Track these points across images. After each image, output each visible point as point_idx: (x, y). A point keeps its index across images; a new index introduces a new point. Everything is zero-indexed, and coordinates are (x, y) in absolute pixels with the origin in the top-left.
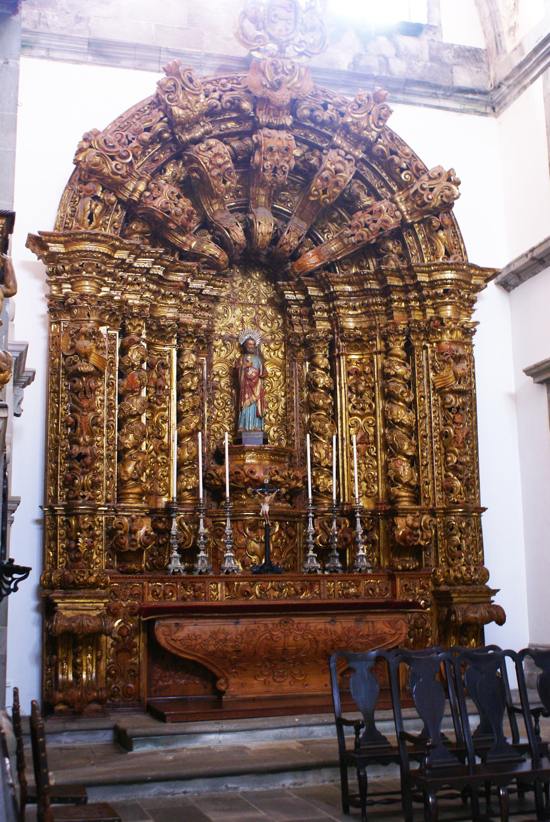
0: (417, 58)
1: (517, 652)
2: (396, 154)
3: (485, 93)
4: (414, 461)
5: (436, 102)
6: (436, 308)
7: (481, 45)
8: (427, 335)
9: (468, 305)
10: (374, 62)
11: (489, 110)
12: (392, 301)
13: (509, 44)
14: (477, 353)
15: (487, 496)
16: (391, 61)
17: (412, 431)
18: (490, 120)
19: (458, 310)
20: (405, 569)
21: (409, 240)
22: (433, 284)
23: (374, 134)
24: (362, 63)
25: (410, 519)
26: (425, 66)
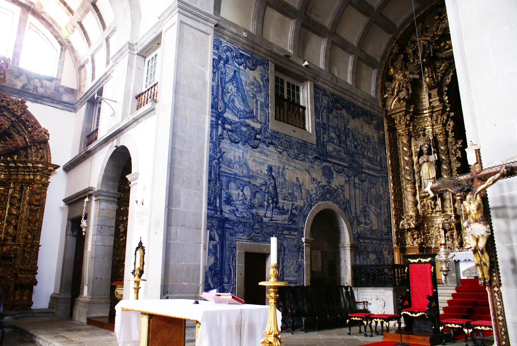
0: (49, 88)
1: (466, 150)
2: (28, 121)
3: (73, 105)
4: (15, 227)
5: (53, 105)
6: (35, 176)
7: (76, 89)
8: (29, 184)
9: (48, 176)
10: (32, 88)
11: (73, 110)
12: (19, 171)
13: (82, 90)
14: (48, 192)
15: (43, 241)
16: (38, 88)
17: (17, 217)
18: (73, 114)
19: (42, 178)
20: (5, 265)
21: (29, 151)
22: (34, 167)
23: (19, 114)
24: (27, 87)
25: (8, 248)
26: (52, 92)
